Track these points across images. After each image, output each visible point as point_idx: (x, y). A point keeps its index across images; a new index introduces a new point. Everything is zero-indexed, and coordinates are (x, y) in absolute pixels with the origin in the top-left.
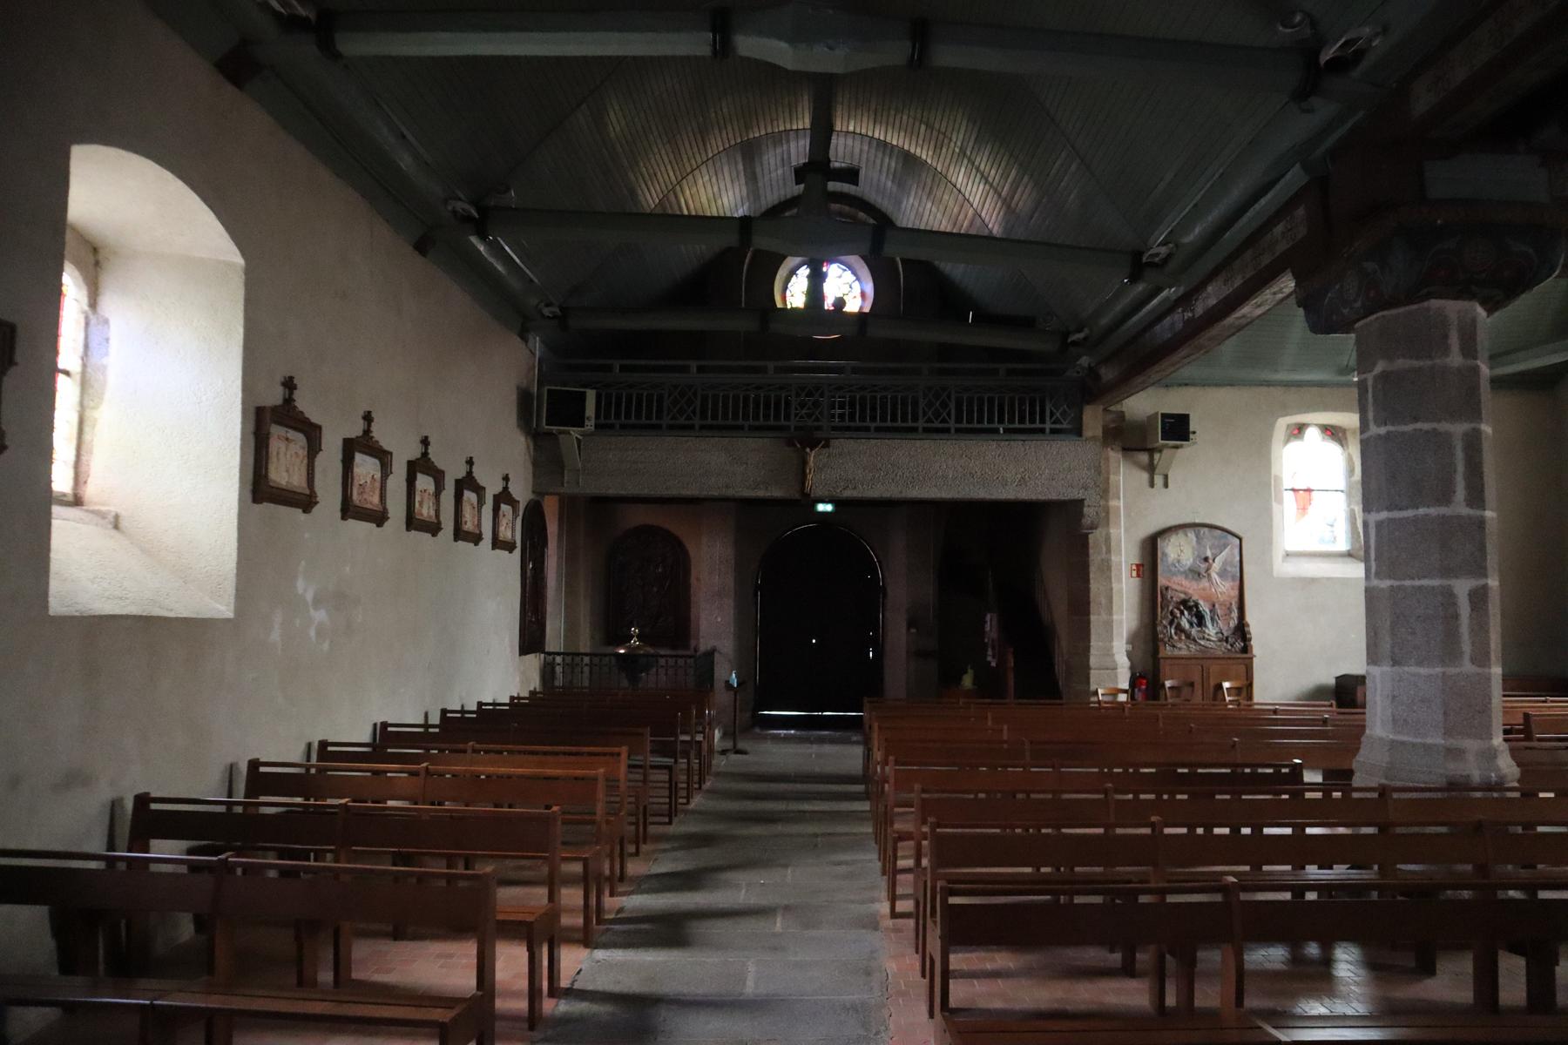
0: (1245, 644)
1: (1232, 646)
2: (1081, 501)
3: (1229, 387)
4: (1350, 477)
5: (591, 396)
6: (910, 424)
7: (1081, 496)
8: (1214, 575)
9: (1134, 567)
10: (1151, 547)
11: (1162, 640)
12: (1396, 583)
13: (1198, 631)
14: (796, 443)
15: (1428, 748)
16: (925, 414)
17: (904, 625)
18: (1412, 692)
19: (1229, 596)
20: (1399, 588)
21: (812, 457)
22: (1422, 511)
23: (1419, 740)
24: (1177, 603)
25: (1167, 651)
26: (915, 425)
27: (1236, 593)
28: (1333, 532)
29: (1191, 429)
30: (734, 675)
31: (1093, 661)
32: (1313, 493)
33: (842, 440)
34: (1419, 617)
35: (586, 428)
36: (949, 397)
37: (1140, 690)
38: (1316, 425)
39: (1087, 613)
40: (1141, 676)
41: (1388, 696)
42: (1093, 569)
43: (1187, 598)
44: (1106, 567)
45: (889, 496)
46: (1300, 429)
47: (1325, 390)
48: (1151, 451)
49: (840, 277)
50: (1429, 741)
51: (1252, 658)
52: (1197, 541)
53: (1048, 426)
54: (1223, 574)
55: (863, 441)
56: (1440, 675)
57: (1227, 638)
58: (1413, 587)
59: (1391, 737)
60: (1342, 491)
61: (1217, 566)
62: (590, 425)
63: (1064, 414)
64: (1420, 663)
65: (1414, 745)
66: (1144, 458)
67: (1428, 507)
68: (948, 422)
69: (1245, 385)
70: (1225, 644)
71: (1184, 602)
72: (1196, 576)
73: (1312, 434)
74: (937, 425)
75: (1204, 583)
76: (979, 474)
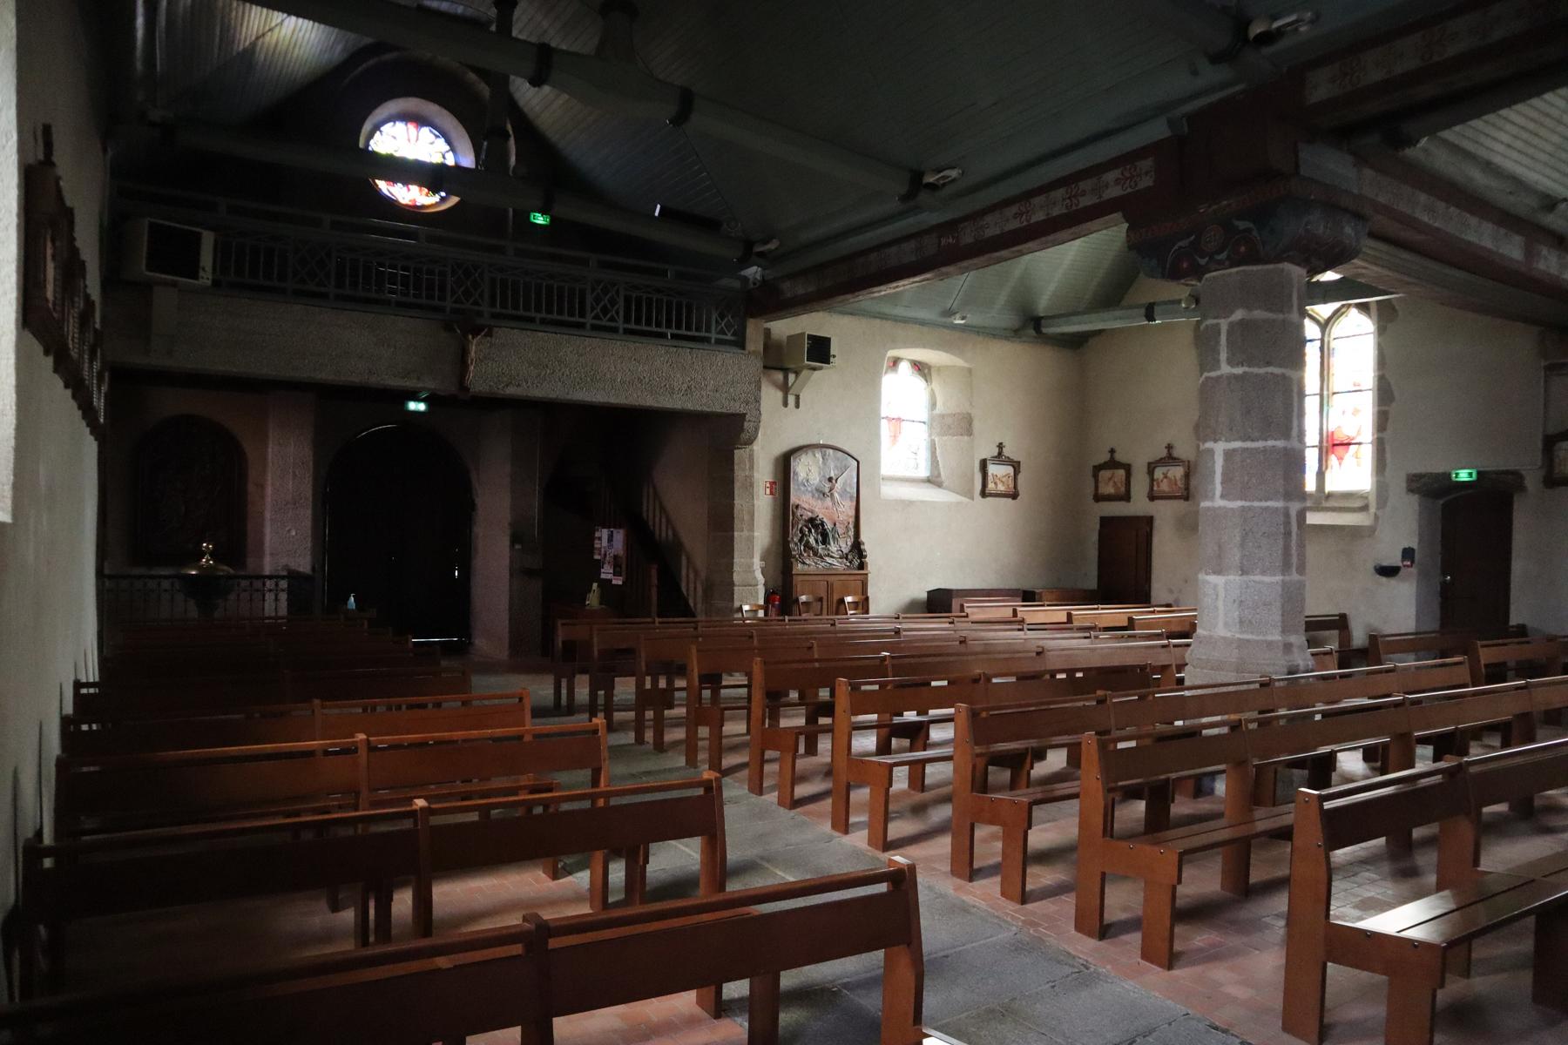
0: (861, 561)
1: (850, 562)
2: (745, 415)
3: (850, 316)
4: (932, 410)
5: (208, 240)
6: (576, 319)
7: (742, 411)
8: (836, 495)
9: (768, 485)
10: (784, 464)
11: (794, 557)
12: (1247, 504)
13: (823, 549)
14: (456, 327)
15: (1270, 644)
16: (593, 309)
17: (506, 541)
18: (1256, 598)
19: (848, 515)
20: (1250, 508)
21: (475, 347)
22: (1270, 443)
23: (1260, 638)
24: (806, 521)
25: (798, 568)
26: (582, 320)
27: (852, 513)
28: (916, 459)
29: (832, 353)
30: (352, 599)
31: (736, 578)
32: (903, 424)
33: (506, 330)
34: (1264, 533)
35: (200, 282)
36: (618, 292)
37: (773, 606)
38: (909, 360)
39: (732, 529)
40: (773, 593)
41: (1234, 601)
42: (737, 485)
43: (814, 516)
44: (749, 485)
45: (554, 396)
46: (896, 362)
47: (925, 329)
48: (786, 371)
49: (432, 143)
50: (1270, 638)
51: (867, 574)
52: (823, 462)
53: (713, 336)
54: (844, 493)
55: (529, 333)
56: (1280, 583)
57: (847, 554)
58: (1261, 508)
59: (1238, 636)
60: (924, 423)
61: (838, 486)
62: (206, 277)
63: (729, 326)
64: (1263, 573)
65: (1257, 642)
66: (779, 376)
67: (1275, 440)
68: (616, 321)
69: (863, 315)
70: (845, 560)
71: (812, 520)
72: (821, 496)
73: (904, 367)
74: (604, 322)
75: (828, 501)
76: (647, 380)
